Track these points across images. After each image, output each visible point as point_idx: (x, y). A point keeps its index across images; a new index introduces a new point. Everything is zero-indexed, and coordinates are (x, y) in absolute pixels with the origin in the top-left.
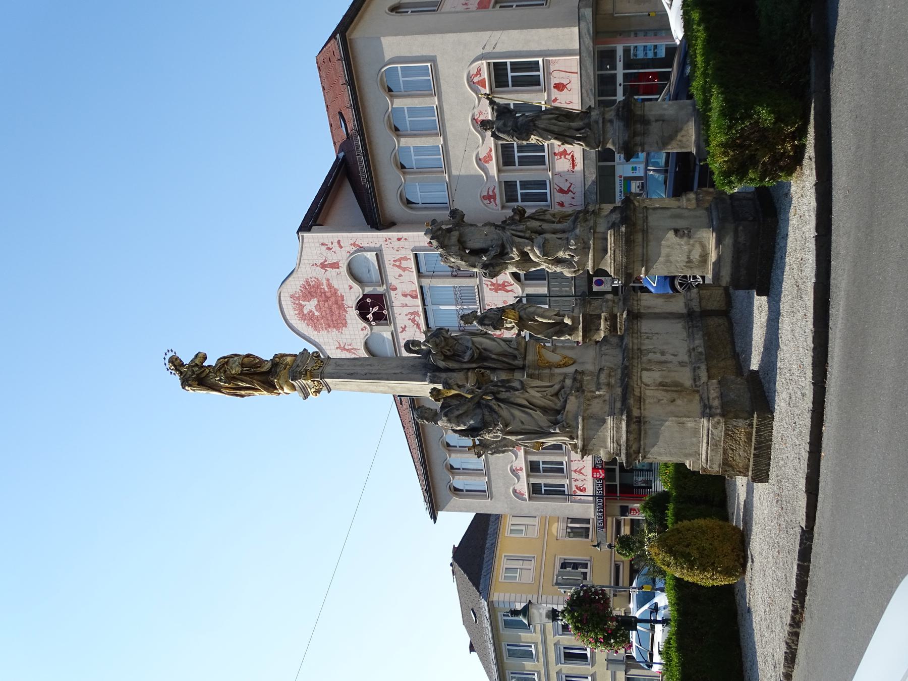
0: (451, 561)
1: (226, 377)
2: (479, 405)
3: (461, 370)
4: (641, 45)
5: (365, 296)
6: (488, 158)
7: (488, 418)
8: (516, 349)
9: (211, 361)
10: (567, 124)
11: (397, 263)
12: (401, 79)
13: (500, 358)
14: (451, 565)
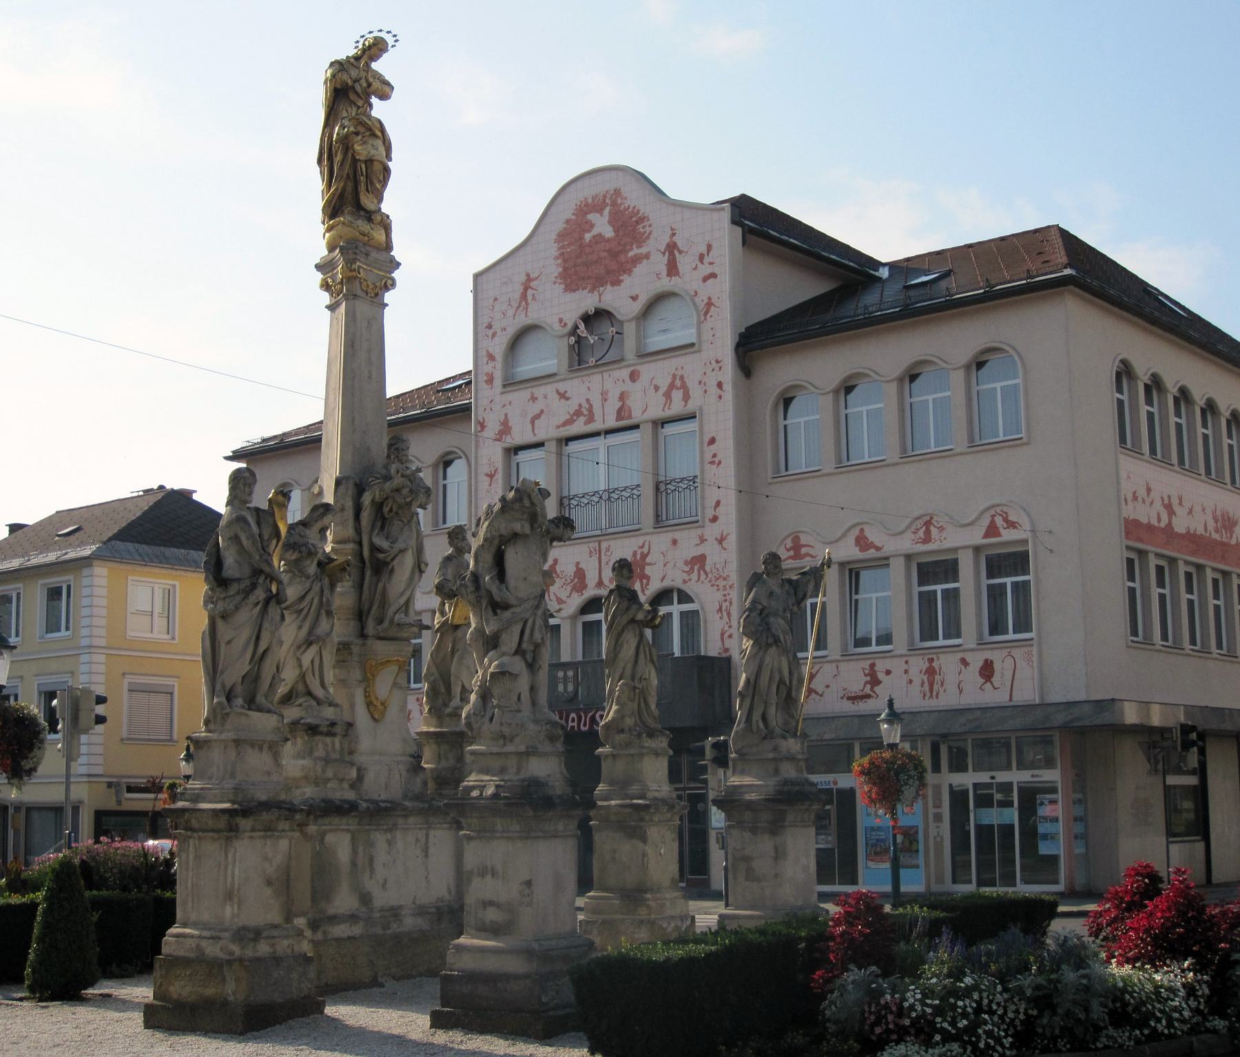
0: (168, 487)
1: (346, 137)
2: (257, 572)
3: (358, 531)
4: (1058, 811)
7: (233, 589)
8: (392, 621)
9: (379, 109)
10: (773, 699)
11: (678, 383)
12: (998, 385)
13: (378, 596)
14: (161, 487)
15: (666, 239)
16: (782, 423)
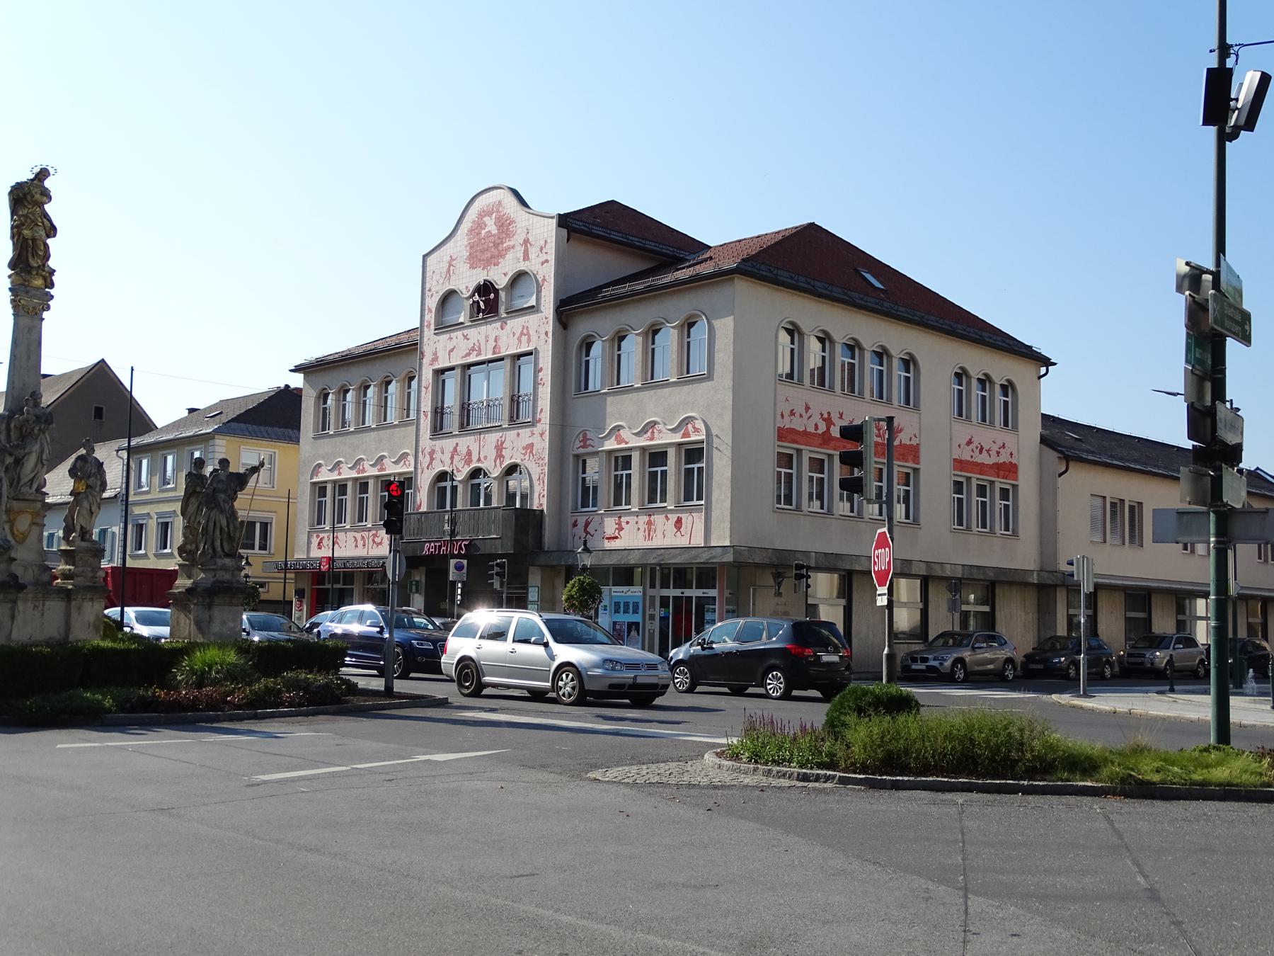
5: (496, 291)
6: (620, 440)
15: (523, 236)
16: (585, 359)
